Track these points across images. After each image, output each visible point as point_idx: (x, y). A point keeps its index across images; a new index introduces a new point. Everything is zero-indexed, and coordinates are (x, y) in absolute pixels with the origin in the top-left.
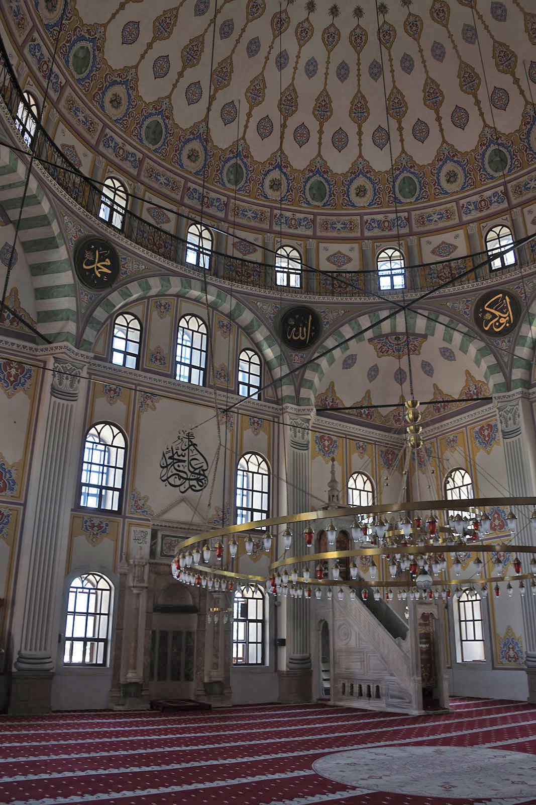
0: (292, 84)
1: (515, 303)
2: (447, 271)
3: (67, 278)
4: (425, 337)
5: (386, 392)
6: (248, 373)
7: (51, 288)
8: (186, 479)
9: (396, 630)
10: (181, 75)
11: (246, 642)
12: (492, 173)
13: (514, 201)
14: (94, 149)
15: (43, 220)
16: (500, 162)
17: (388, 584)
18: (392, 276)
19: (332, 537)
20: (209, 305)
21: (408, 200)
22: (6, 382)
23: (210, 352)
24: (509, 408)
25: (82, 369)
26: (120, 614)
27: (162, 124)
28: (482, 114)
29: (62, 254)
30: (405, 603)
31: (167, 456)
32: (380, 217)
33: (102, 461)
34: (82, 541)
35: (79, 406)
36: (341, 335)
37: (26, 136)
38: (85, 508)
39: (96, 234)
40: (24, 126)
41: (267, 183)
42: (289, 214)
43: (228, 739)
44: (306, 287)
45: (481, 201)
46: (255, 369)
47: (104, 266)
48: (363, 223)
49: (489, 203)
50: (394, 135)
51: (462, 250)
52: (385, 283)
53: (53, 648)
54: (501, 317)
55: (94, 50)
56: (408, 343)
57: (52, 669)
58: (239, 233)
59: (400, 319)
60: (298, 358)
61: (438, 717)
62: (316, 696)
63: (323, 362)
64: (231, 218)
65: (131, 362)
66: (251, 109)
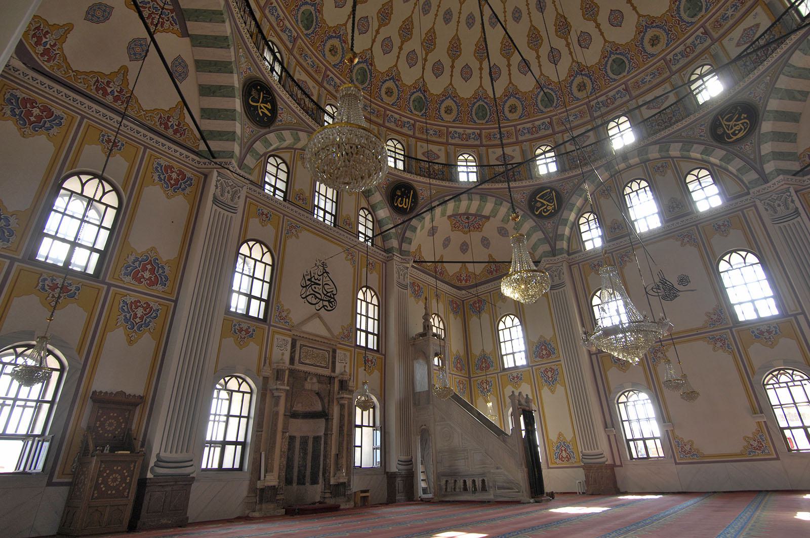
6: (365, 228)
8: (321, 300)
12: (542, 108)
14: (321, 85)
21: (481, 122)
22: (165, 183)
24: (554, 269)
25: (242, 188)
27: (314, 15)
31: (307, 278)
33: (249, 282)
34: (230, 341)
39: (263, 79)
41: (383, 90)
45: (533, 128)
47: (266, 107)
48: (448, 133)
49: (539, 129)
54: (548, 205)
55: (316, 12)
57: (192, 473)
65: (279, 195)
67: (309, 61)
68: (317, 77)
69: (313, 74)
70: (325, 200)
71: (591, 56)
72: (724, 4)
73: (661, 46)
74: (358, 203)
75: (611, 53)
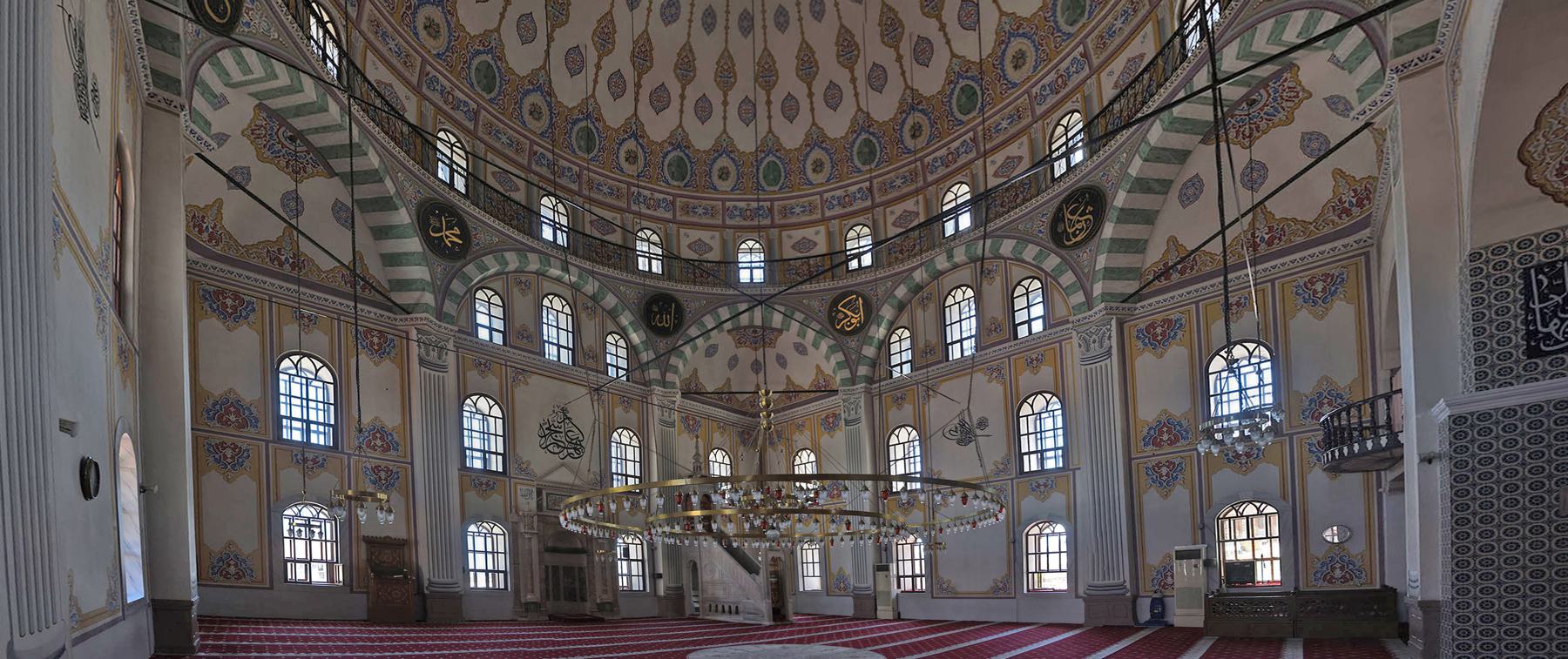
0: (646, 31)
1: (867, 304)
2: (805, 267)
3: (414, 244)
4: (780, 331)
5: (744, 380)
6: (616, 355)
7: (399, 255)
9: (751, 568)
10: (682, 97)
11: (630, 576)
12: (859, 165)
13: (878, 200)
14: (416, 90)
15: (373, 176)
16: (869, 154)
17: (745, 536)
18: (751, 269)
19: (695, 500)
20: (572, 286)
23: (576, 332)
26: (514, 552)
28: (856, 95)
29: (403, 217)
30: (759, 549)
32: (742, 205)
33: (481, 429)
34: (471, 496)
35: (450, 378)
36: (704, 325)
37: (330, 64)
38: (472, 469)
40: (324, 50)
41: (622, 155)
42: (647, 193)
43: (620, 640)
44: (667, 274)
46: (623, 353)
48: (725, 210)
49: (853, 198)
50: (761, 110)
51: (822, 248)
52: (744, 276)
53: (458, 575)
56: (762, 337)
58: (595, 210)
59: (758, 312)
60: (663, 344)
61: (784, 626)
62: (688, 613)
63: (687, 350)
64: (586, 192)
65: (498, 339)
66: (600, 58)
67: (504, 139)
68: (520, 160)
69: (514, 156)
70: (556, 330)
71: (930, 81)
72: (1116, 4)
73: (921, 141)
74: (603, 326)
75: (959, 75)
